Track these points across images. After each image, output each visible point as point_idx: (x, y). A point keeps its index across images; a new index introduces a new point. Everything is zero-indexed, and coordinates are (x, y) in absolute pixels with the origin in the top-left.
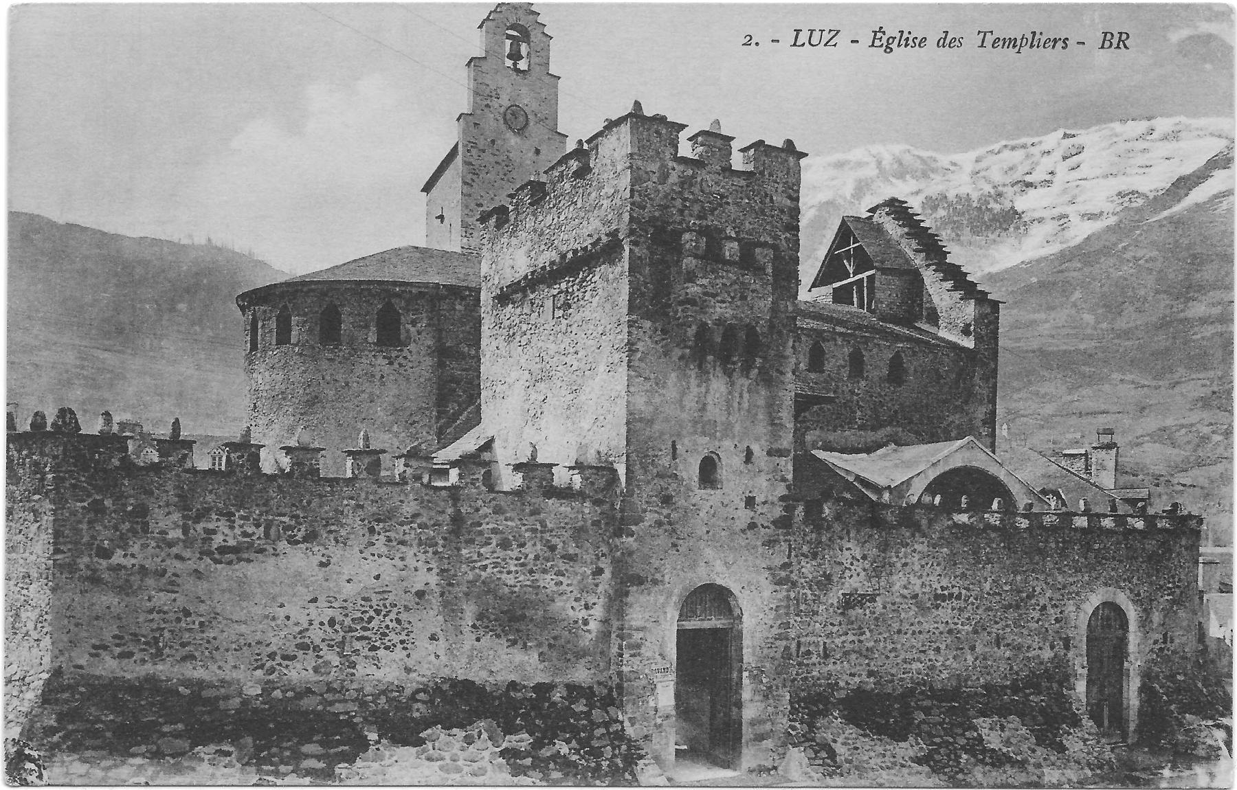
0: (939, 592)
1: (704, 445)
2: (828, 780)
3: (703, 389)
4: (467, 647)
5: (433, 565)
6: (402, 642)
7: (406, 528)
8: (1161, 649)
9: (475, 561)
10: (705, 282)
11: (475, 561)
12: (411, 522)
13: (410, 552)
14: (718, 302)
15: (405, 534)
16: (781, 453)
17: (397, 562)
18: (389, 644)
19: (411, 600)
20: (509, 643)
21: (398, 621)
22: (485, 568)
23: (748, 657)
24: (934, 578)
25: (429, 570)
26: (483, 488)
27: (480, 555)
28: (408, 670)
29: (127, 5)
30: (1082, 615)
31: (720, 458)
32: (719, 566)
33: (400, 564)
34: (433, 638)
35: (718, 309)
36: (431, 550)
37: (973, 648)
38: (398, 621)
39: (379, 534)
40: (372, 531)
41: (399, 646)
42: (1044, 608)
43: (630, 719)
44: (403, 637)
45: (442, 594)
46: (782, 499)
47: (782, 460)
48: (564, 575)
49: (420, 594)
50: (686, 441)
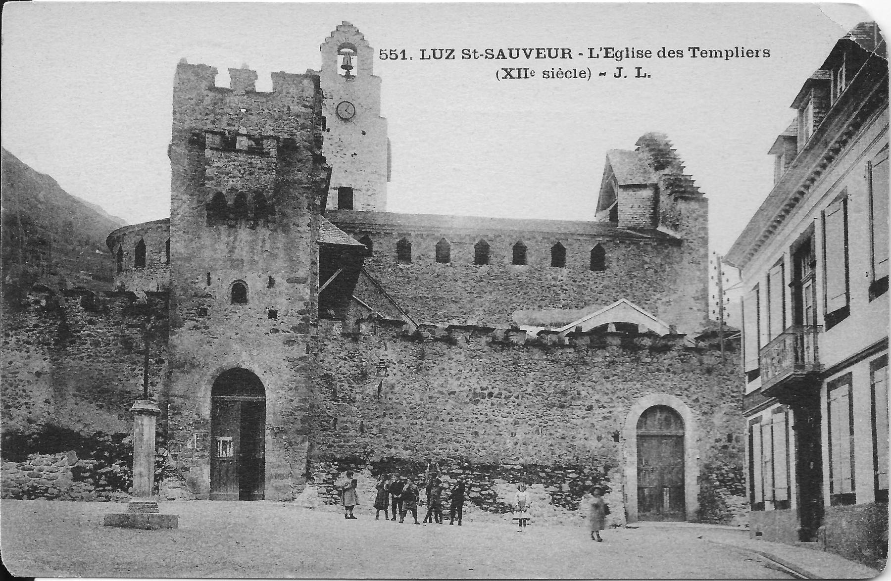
0: (478, 390)
1: (234, 276)
2: (329, 507)
3: (232, 238)
4: (69, 407)
5: (48, 356)
6: (26, 403)
7: (30, 333)
8: (725, 447)
9: (76, 354)
10: (220, 164)
11: (76, 354)
12: (33, 330)
13: (32, 348)
14: (231, 177)
15: (28, 337)
16: (298, 281)
17: (23, 353)
18: (17, 405)
19: (32, 378)
20: (98, 408)
21: (24, 391)
22: (82, 359)
23: (270, 419)
24: (474, 380)
25: (45, 359)
26: (81, 308)
27: (78, 350)
28: (30, 421)
29: (751, 4)
30: (630, 415)
31: (245, 283)
32: (245, 356)
33: (25, 355)
34: (47, 401)
35: (231, 183)
36: (46, 347)
37: (513, 435)
38: (24, 391)
39: (12, 336)
40: (7, 335)
41: (24, 407)
42: (590, 408)
43: (173, 456)
44: (27, 400)
45: (53, 374)
46: (300, 313)
47: (300, 286)
48: (137, 364)
49: (38, 374)
50: (219, 272)
